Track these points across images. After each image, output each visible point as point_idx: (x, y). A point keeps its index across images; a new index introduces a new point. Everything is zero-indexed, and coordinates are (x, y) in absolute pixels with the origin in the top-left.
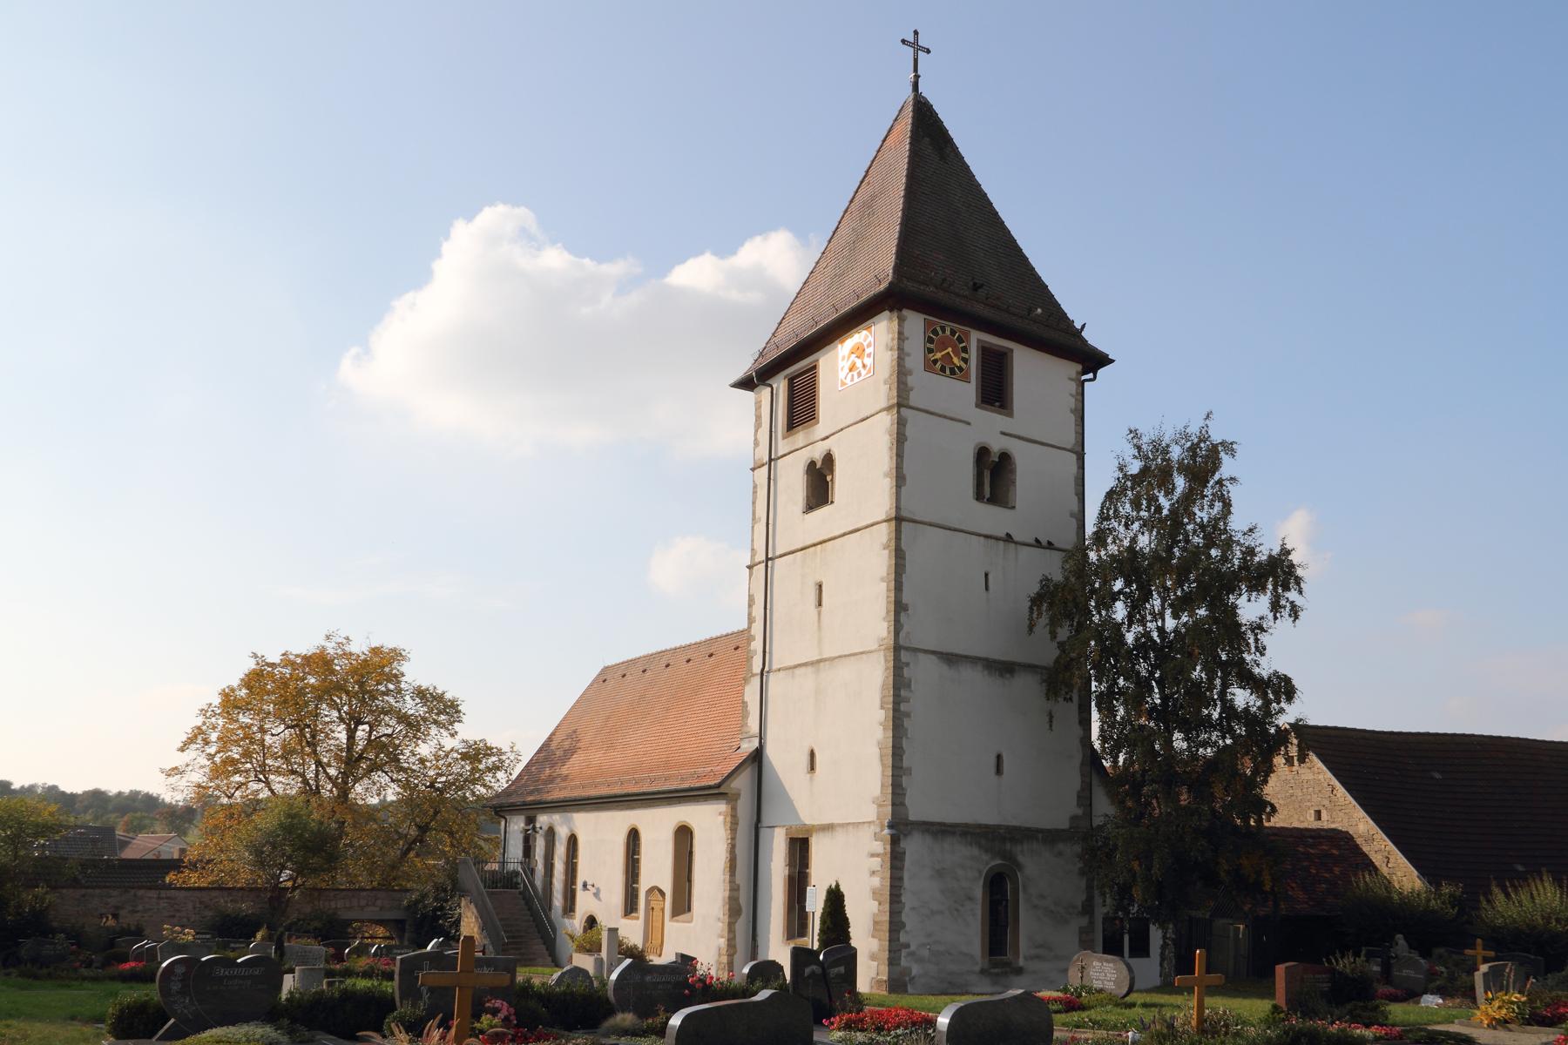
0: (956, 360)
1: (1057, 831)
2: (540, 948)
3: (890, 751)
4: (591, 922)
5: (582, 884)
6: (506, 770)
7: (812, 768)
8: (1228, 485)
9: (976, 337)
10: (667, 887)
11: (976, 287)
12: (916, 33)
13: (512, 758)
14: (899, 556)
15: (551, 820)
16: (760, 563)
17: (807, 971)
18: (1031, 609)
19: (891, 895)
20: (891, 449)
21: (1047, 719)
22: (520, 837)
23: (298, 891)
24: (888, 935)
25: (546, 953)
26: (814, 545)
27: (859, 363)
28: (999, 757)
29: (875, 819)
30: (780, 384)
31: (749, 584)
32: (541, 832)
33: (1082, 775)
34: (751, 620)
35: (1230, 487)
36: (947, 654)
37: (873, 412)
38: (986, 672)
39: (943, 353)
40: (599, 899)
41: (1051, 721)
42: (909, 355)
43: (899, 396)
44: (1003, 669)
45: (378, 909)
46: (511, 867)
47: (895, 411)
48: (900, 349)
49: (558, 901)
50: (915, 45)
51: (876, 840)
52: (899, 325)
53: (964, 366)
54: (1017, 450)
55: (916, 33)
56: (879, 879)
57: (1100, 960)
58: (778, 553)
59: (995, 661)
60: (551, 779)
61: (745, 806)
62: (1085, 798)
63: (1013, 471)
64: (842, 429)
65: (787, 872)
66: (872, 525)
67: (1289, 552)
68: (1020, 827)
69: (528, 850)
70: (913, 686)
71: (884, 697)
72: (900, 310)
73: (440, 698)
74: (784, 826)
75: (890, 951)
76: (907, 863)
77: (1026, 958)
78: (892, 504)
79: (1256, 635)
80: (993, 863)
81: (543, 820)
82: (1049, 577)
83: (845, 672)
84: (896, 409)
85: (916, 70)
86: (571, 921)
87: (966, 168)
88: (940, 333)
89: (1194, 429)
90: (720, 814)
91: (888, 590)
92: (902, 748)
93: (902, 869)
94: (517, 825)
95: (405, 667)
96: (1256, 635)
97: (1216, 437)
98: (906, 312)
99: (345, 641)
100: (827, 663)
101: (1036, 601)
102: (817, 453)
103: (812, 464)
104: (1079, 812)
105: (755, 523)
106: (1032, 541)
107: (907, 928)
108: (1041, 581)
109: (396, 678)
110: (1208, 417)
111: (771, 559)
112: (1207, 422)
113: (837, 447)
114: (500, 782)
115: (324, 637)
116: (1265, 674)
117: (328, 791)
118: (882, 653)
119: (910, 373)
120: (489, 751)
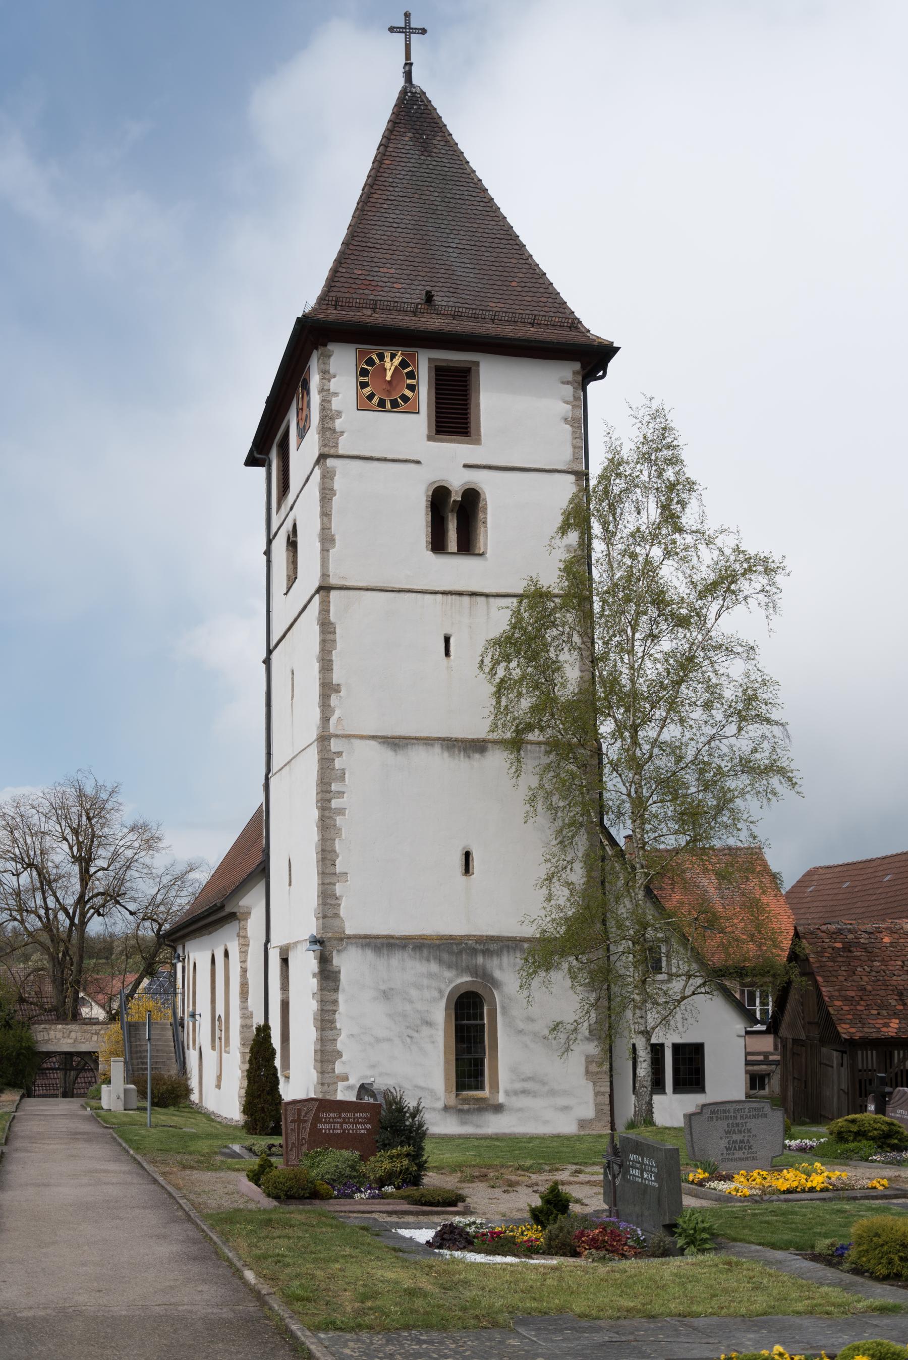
54: (484, 481)
77: (507, 1093)
92: (335, 851)
107: (344, 1058)
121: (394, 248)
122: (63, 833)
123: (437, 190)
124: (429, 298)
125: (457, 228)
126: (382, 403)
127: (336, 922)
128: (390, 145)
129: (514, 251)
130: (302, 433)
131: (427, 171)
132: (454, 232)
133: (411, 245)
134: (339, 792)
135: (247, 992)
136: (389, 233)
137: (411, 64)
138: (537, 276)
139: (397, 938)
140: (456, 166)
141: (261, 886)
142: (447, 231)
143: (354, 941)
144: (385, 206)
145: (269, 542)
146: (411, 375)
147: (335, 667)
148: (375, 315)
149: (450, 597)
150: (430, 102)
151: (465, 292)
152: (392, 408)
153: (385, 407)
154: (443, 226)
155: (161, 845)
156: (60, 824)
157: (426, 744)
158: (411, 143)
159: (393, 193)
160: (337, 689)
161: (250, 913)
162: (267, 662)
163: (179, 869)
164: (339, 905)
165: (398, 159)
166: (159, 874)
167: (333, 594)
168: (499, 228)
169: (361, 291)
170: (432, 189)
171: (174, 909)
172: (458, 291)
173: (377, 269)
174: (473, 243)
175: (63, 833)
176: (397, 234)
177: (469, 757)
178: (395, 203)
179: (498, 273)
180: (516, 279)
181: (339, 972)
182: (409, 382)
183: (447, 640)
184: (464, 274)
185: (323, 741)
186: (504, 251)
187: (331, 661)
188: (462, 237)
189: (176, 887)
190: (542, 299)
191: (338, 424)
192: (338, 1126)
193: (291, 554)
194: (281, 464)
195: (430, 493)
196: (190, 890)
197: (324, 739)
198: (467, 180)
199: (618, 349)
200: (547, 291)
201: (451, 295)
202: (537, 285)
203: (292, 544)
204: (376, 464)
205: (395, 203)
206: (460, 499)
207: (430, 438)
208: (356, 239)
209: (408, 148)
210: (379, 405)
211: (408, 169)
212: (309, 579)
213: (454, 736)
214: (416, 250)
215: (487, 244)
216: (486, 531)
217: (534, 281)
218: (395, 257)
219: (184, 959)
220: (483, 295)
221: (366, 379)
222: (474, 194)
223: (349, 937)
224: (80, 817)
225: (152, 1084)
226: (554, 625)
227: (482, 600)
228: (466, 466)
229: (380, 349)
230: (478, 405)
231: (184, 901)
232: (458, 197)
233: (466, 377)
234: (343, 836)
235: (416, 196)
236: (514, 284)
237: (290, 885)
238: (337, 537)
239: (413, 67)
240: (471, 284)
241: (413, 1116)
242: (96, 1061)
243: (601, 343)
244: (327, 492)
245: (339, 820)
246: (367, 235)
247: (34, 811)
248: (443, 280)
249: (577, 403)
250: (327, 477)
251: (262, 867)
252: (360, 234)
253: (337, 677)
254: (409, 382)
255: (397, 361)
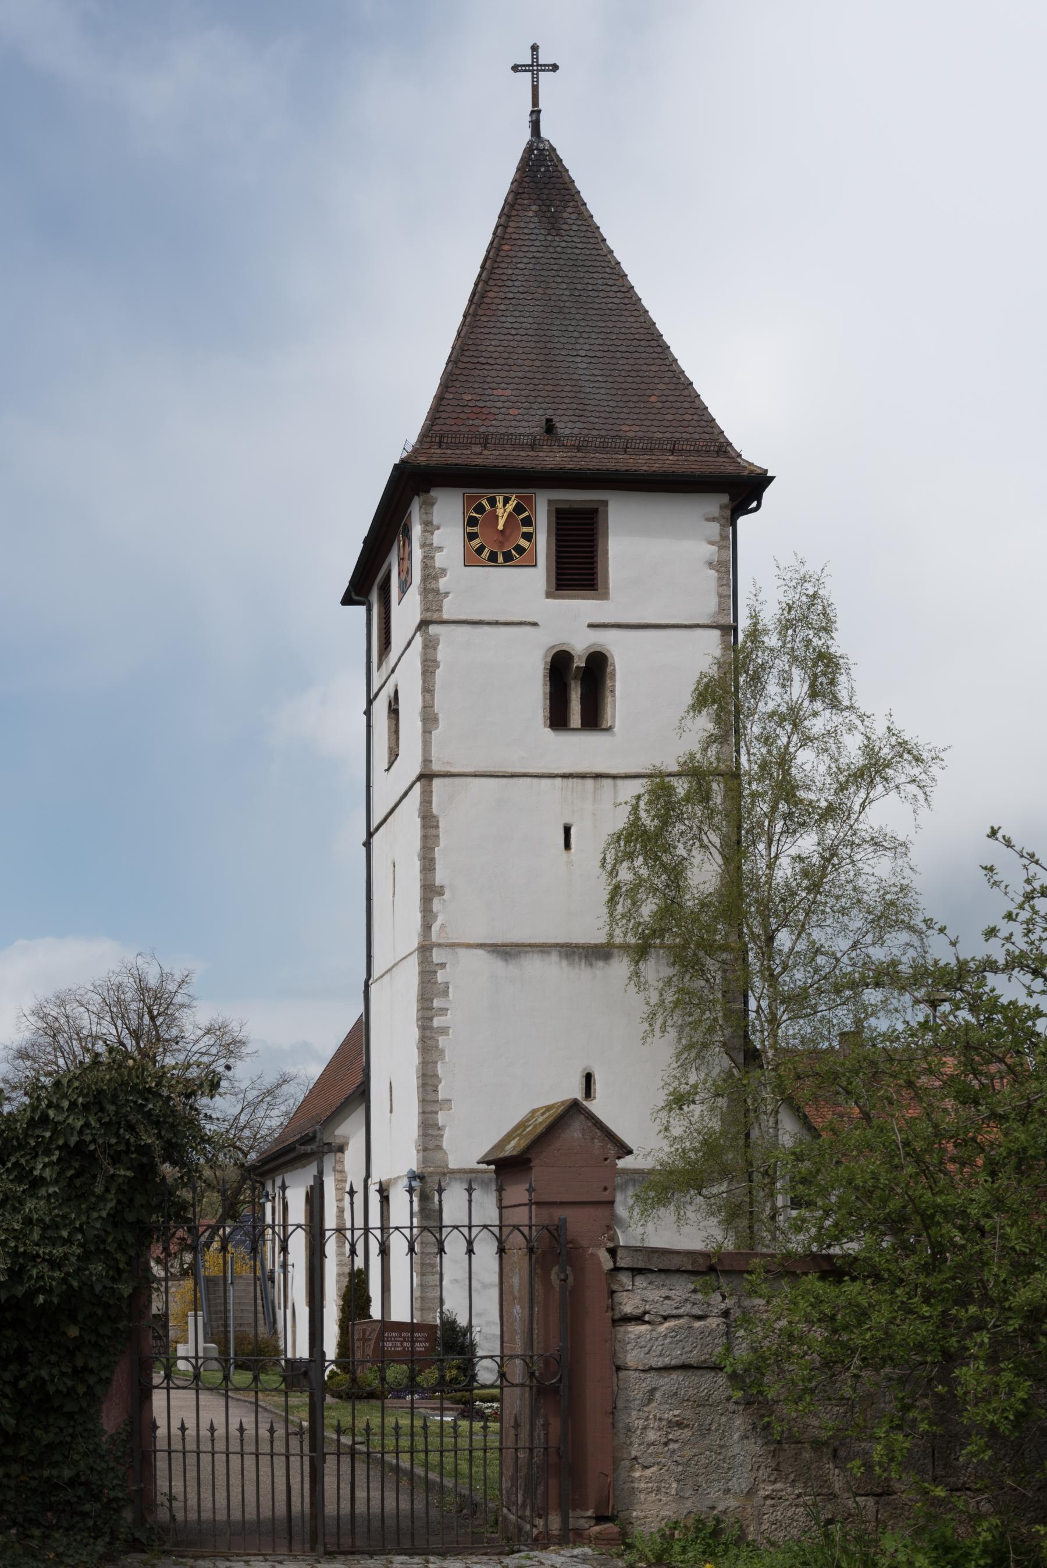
54: (613, 643)
92: (437, 1076)
121: (511, 362)
122: (119, 1036)
123: (566, 280)
124: (550, 427)
125: (587, 329)
126: (493, 557)
127: (438, 1155)
128: (511, 224)
129: (656, 355)
130: (404, 587)
131: (554, 256)
132: (585, 335)
133: (533, 357)
134: (442, 1009)
136: (505, 343)
137: (539, 112)
138: (682, 387)
140: (590, 246)
141: (361, 1112)
142: (576, 334)
143: (458, 1176)
144: (502, 307)
145: (370, 702)
146: (527, 522)
147: (438, 867)
148: (485, 452)
149: (570, 780)
150: (561, 160)
151: (593, 414)
152: (505, 561)
153: (496, 561)
154: (571, 328)
155: (245, 1050)
156: (115, 1025)
157: (542, 952)
158: (536, 220)
159: (511, 289)
160: (440, 891)
161: (348, 1144)
162: (367, 844)
163: (270, 1080)
164: (442, 1136)
165: (520, 242)
166: (243, 1088)
167: (436, 782)
168: (639, 325)
169: (471, 422)
170: (559, 280)
171: (263, 1133)
172: (586, 413)
173: (490, 392)
174: (606, 348)
175: (119, 1036)
176: (514, 343)
177: (591, 965)
178: (514, 302)
179: (634, 386)
180: (656, 392)
182: (525, 529)
183: (567, 830)
184: (594, 390)
185: (423, 951)
186: (643, 355)
187: (433, 859)
188: (593, 341)
189: (265, 1106)
190: (686, 417)
191: (443, 583)
192: (398, 1344)
193: (394, 722)
194: (382, 609)
195: (549, 660)
196: (283, 1108)
197: (425, 949)
198: (603, 264)
199: (772, 478)
200: (692, 405)
201: (577, 419)
202: (682, 399)
203: (394, 711)
204: (486, 629)
205: (514, 302)
206: (583, 665)
207: (549, 595)
208: (467, 353)
209: (532, 226)
210: (489, 560)
211: (530, 255)
212: (410, 764)
213: (574, 941)
214: (538, 363)
215: (624, 349)
216: (614, 701)
217: (678, 393)
218: (512, 374)
219: (274, 1198)
220: (615, 416)
221: (475, 529)
222: (610, 282)
223: (453, 1172)
224: (141, 1017)
225: (236, 1344)
226: (680, 818)
227: (608, 782)
228: (591, 626)
229: (490, 492)
230: (606, 552)
231: (275, 1123)
232: (590, 287)
233: (592, 519)
234: (447, 1059)
235: (540, 290)
236: (653, 399)
237: (391, 1112)
238: (441, 716)
239: (542, 115)
240: (601, 403)
241: (465, 1335)
242: (165, 1326)
243: (752, 472)
244: (430, 664)
245: (442, 1041)
246: (479, 348)
247: (82, 1009)
248: (567, 400)
249: (724, 543)
250: (430, 646)
251: (361, 1089)
252: (471, 348)
253: (440, 877)
254: (525, 529)
255: (510, 507)
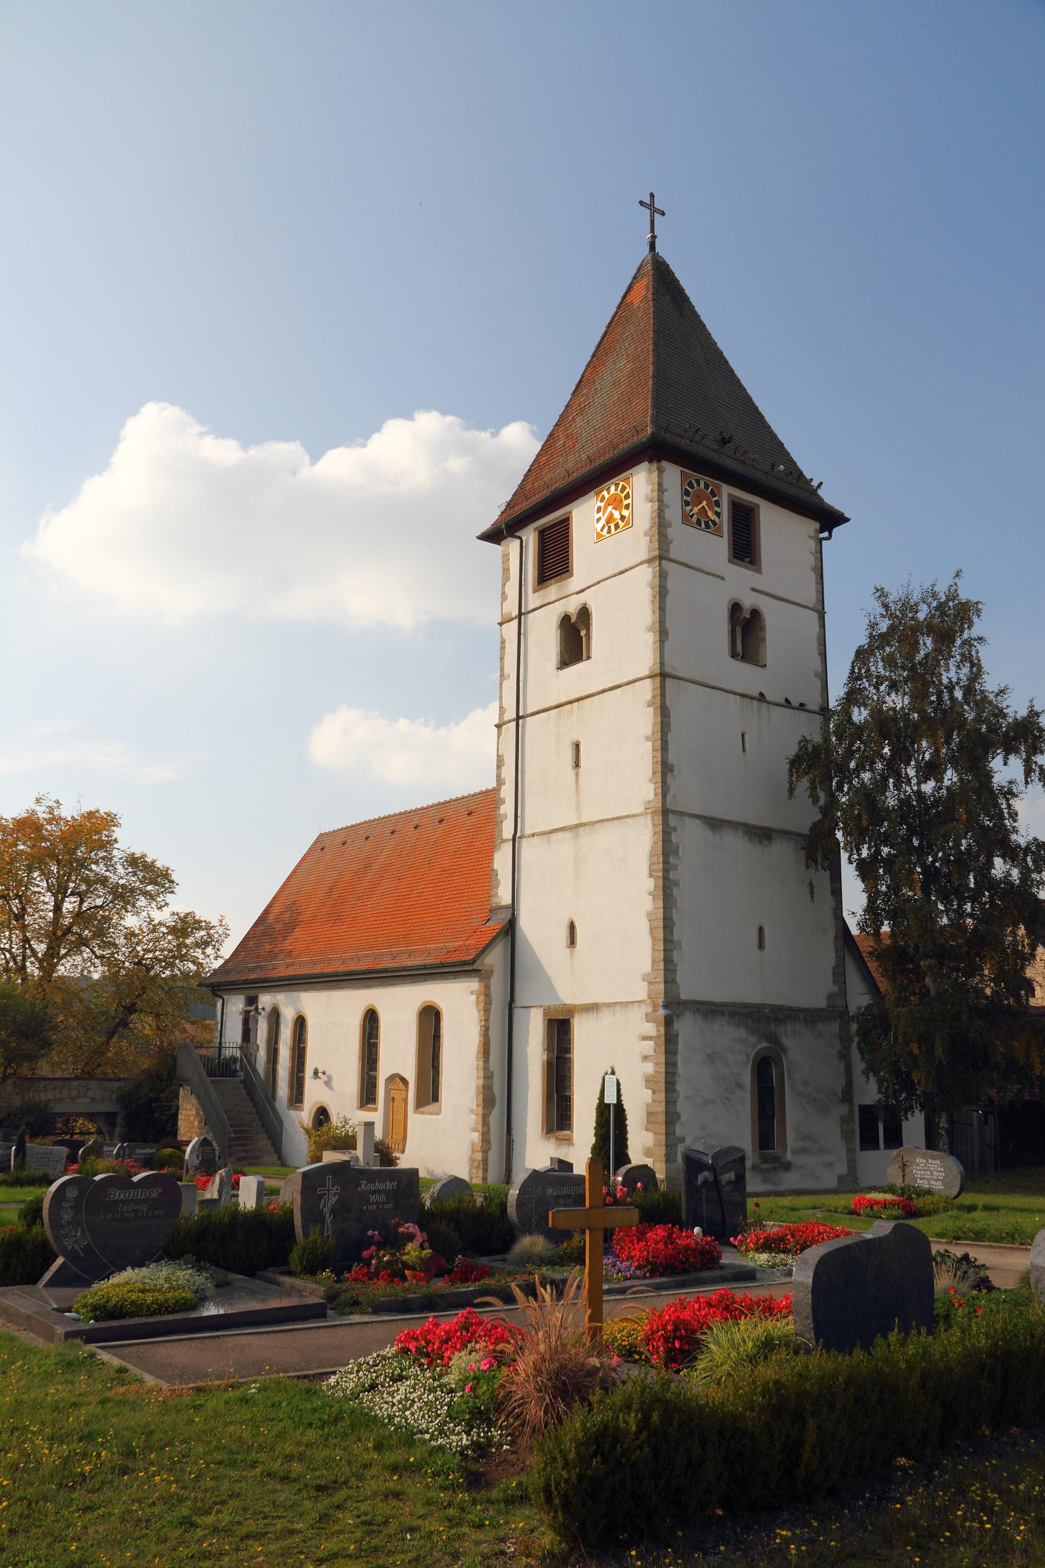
0: (710, 513)
1: (816, 1010)
2: (265, 1143)
3: (661, 924)
4: (322, 1115)
5: (313, 1071)
6: (215, 946)
7: (572, 942)
8: (975, 643)
9: (727, 491)
10: (411, 1075)
11: (724, 441)
12: (652, 195)
13: (220, 932)
14: (664, 713)
15: (275, 1001)
16: (510, 721)
17: (701, 1178)
18: (790, 771)
19: (666, 1082)
20: (653, 602)
21: (808, 889)
22: (239, 1019)
23: (10, 1081)
24: (664, 1127)
25: (272, 1149)
26: (570, 702)
27: (617, 515)
28: (761, 930)
29: (645, 997)
30: (530, 536)
31: (498, 744)
32: (263, 1013)
33: (837, 950)
34: (500, 781)
35: (979, 647)
36: (711, 819)
37: (632, 564)
38: (746, 838)
39: (699, 507)
40: (332, 1089)
41: (812, 892)
42: (668, 507)
43: (660, 548)
44: (762, 835)
45: (89, 1100)
46: (227, 1053)
47: (657, 564)
48: (660, 500)
49: (283, 1089)
50: (650, 206)
51: (647, 1021)
52: (659, 476)
53: (717, 520)
54: (767, 608)
55: (652, 195)
56: (652, 1064)
57: (924, 1156)
58: (529, 711)
59: (754, 827)
60: (273, 955)
61: (498, 983)
62: (839, 975)
63: (763, 629)
64: (599, 582)
65: (545, 1057)
66: (635, 681)
67: (1038, 714)
68: (783, 1006)
69: (247, 1034)
70: (680, 853)
71: (653, 864)
72: (659, 461)
73: (149, 867)
74: (541, 1006)
75: (667, 1146)
76: (681, 1047)
77: (793, 1152)
78: (655, 660)
79: (1008, 800)
80: (760, 1046)
81: (266, 1000)
82: (809, 738)
83: (607, 836)
84: (658, 562)
85: (652, 230)
86: (298, 1112)
87: (703, 326)
88: (695, 485)
89: (942, 589)
90: (472, 993)
91: (654, 750)
92: (672, 919)
93: (675, 1053)
94: (235, 1005)
95: (117, 833)
96: (1008, 800)
97: (964, 596)
98: (664, 464)
99: (55, 805)
100: (587, 827)
101: (795, 763)
102: (572, 606)
103: (566, 619)
104: (835, 989)
105: (504, 680)
106: (783, 702)
107: (683, 1119)
108: (800, 742)
109: (108, 844)
110: (957, 575)
111: (523, 717)
112: (957, 580)
113: (592, 599)
114: (213, 961)
115: (33, 800)
116: (1022, 842)
117: (33, 969)
118: (649, 816)
119: (669, 525)
120: (197, 925)
135: (489, 1052)
139: (718, 1005)
181: (677, 1036)
239: (657, 240)
